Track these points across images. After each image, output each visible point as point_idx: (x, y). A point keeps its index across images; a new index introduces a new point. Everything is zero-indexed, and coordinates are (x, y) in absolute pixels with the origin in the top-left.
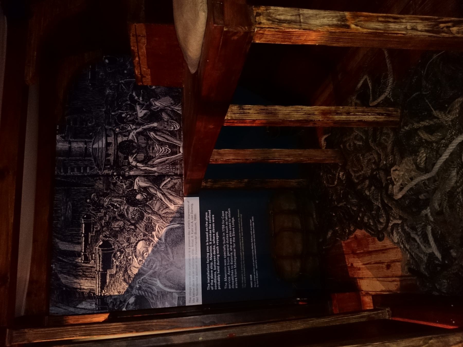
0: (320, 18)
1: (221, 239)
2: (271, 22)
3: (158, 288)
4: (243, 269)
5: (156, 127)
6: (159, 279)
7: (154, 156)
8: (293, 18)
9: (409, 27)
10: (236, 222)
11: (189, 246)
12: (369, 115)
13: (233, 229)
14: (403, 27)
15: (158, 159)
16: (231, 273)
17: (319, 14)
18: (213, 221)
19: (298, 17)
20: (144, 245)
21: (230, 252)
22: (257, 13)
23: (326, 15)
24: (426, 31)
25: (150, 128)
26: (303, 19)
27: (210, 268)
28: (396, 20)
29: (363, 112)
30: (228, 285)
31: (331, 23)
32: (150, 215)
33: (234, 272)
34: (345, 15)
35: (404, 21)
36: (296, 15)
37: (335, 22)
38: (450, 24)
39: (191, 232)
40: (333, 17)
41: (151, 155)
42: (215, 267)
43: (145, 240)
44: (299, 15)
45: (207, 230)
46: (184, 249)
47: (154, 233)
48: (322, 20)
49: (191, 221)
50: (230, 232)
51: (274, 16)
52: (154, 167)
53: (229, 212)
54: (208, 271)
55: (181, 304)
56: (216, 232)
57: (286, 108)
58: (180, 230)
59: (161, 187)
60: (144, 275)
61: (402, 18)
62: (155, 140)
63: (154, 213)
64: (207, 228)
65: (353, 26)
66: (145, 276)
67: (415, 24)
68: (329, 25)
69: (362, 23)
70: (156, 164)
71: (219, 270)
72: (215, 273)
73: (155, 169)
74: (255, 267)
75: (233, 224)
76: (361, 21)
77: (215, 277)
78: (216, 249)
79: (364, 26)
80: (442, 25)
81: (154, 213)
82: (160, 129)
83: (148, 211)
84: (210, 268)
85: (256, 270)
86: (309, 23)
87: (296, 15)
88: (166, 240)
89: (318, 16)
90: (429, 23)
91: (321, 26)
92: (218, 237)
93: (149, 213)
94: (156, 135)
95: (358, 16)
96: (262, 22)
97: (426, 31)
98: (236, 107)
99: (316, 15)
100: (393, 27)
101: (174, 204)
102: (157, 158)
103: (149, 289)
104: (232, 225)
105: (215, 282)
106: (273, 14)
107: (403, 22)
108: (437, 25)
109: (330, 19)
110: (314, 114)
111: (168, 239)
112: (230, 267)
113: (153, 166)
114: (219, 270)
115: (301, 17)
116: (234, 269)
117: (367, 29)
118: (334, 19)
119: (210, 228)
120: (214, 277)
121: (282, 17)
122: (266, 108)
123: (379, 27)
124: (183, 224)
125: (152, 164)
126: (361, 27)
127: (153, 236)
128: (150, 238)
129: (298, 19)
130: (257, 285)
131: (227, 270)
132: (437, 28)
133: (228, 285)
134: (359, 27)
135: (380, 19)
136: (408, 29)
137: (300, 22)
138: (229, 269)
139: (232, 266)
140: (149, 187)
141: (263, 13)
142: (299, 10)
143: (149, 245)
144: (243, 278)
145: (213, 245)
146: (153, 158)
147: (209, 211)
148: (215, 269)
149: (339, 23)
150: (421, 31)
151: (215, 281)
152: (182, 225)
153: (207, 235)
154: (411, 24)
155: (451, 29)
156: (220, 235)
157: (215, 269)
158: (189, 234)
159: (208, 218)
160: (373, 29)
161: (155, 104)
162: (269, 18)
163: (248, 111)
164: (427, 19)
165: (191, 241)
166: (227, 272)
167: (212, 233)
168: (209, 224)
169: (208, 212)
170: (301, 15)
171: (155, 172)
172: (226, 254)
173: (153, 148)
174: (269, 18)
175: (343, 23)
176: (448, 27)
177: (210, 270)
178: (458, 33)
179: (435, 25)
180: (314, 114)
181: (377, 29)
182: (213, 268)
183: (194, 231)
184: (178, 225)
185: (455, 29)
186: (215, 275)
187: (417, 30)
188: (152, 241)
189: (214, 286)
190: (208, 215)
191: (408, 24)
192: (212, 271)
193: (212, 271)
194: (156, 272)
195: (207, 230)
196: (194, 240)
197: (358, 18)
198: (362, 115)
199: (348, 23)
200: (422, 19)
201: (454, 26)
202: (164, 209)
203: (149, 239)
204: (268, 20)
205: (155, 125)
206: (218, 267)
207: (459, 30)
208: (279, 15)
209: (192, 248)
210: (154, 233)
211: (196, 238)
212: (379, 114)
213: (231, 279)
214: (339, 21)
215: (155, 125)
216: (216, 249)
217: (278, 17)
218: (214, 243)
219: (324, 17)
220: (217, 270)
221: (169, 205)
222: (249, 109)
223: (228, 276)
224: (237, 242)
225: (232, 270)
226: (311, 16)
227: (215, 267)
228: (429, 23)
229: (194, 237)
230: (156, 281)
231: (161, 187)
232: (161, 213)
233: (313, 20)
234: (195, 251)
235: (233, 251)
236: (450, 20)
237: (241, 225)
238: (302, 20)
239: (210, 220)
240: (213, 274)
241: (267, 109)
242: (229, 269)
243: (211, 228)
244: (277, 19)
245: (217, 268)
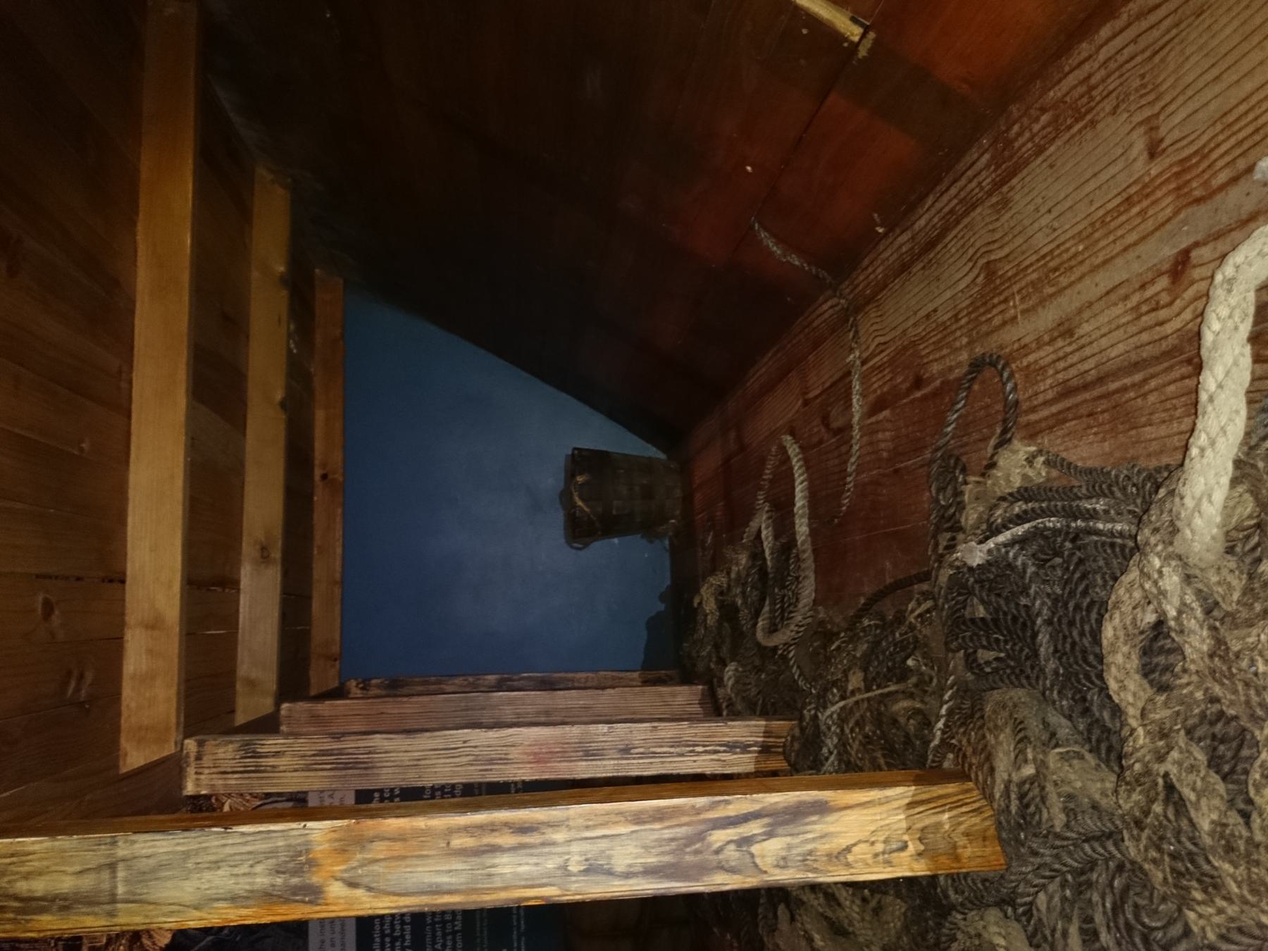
0: (198, 868)
4: (482, 932)
12: (699, 753)
14: (551, 864)
19: (106, 875)
23: (228, 850)
26: (127, 881)
27: (382, 931)
28: (526, 839)
29: (676, 743)
31: (242, 886)
33: (455, 943)
34: (308, 843)
35: (559, 836)
36: (98, 869)
37: (262, 881)
38: (754, 828)
42: (398, 927)
44: (112, 867)
48: (207, 875)
54: (378, 940)
57: (408, 741)
65: (336, 890)
67: (603, 844)
71: (408, 937)
72: (398, 944)
74: (519, 928)
79: (382, 886)
80: (719, 837)
84: (382, 931)
86: (151, 898)
90: (667, 834)
91: (196, 908)
97: (649, 872)
98: (231, 747)
99: (187, 855)
100: (507, 870)
107: (554, 844)
108: (700, 836)
109: (244, 869)
110: (505, 761)
112: (444, 928)
114: (408, 937)
115: (121, 874)
116: (454, 933)
117: (395, 894)
122: (336, 746)
123: (445, 879)
126: (370, 889)
129: (106, 886)
131: (434, 936)
132: (697, 852)
134: (359, 892)
135: (458, 842)
136: (570, 874)
137: (113, 899)
138: (439, 933)
139: (449, 926)
142: (114, 843)
148: (397, 934)
149: (279, 880)
150: (627, 875)
154: (586, 846)
155: (755, 849)
157: (397, 934)
163: (271, 761)
164: (659, 816)
166: (434, 943)
170: (121, 866)
175: (295, 881)
176: (745, 841)
177: (383, 936)
178: (783, 863)
179: (690, 840)
180: (505, 761)
182: (393, 930)
185: (774, 846)
187: (610, 873)
192: (387, 940)
193: (387, 940)
197: (363, 849)
198: (671, 754)
206: (408, 928)
207: (789, 847)
212: (731, 747)
217: (22, 887)
219: (216, 865)
220: (403, 936)
222: (277, 754)
225: (450, 937)
226: (161, 866)
227: (398, 927)
233: (169, 884)
236: (757, 807)
238: (121, 890)
241: (341, 752)
242: (439, 933)
244: (16, 898)
245: (402, 930)
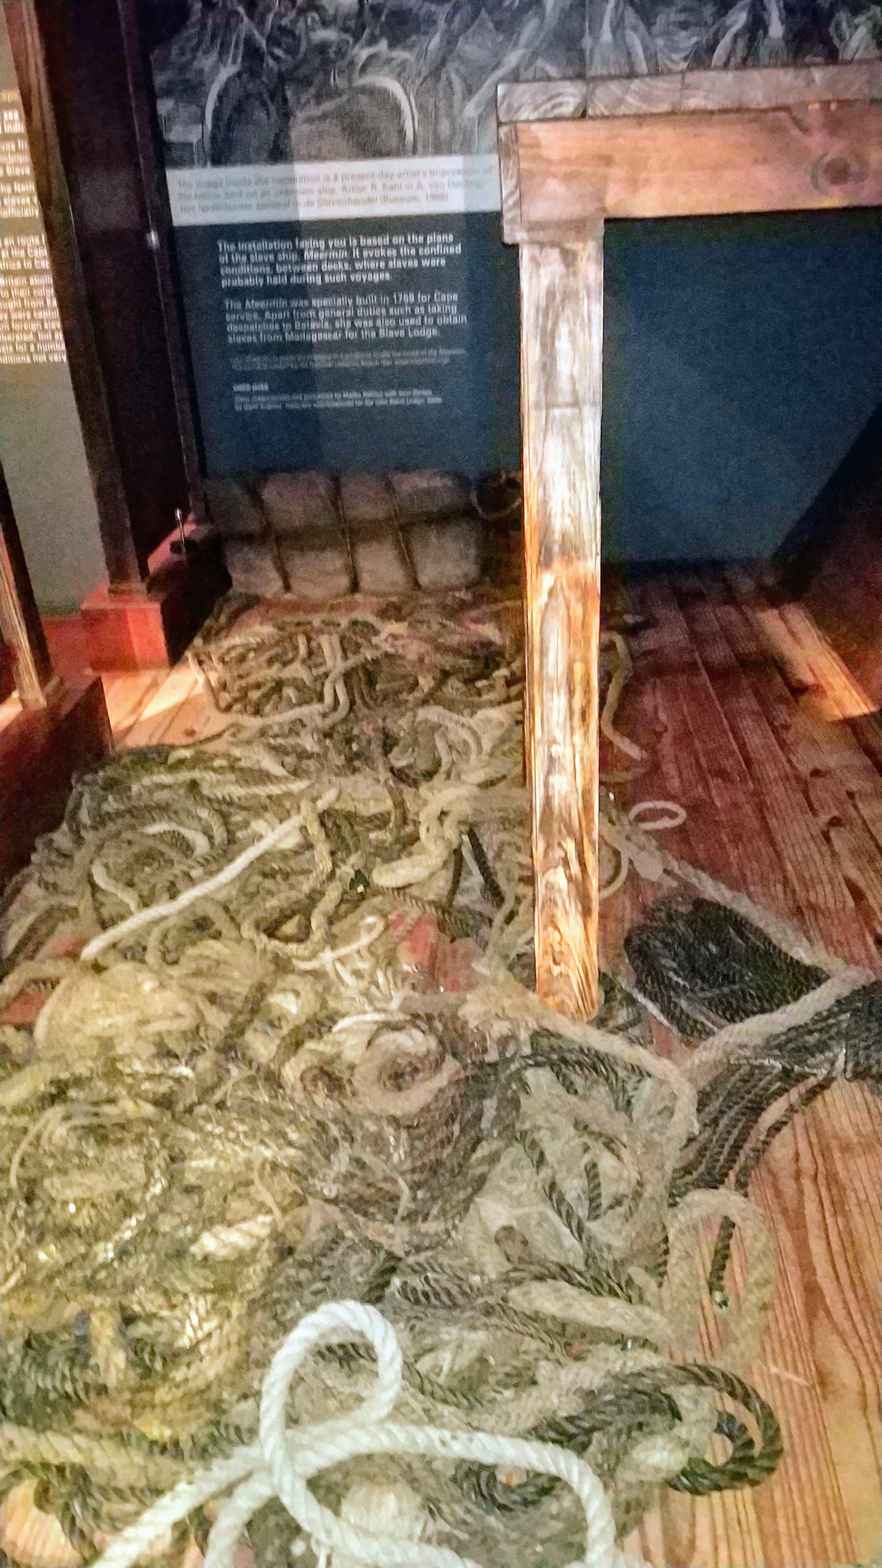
1: (365, 289)
2: (543, 303)
3: (215, 70)
5: (766, 31)
6: (239, 75)
7: (656, 29)
8: (563, 383)
9: (555, 750)
10: (421, 343)
11: (345, 177)
13: (402, 333)
15: (646, 49)
16: (269, 321)
17: (583, 472)
18: (425, 263)
20: (344, 10)
21: (332, 320)
22: (575, 255)
23: (583, 496)
24: (548, 801)
25: (764, 9)
26: (563, 416)
30: (235, 312)
32: (442, 24)
33: (274, 332)
35: (578, 738)
36: (574, 392)
38: (575, 869)
39: (389, 182)
40: (577, 520)
41: (661, 20)
43: (360, 13)
44: (576, 403)
45: (395, 241)
46: (335, 155)
47: (383, 45)
48: (564, 480)
49: (425, 182)
50: (392, 322)
51: (568, 312)
52: (614, 32)
53: (456, 321)
55: (175, 154)
56: (393, 271)
58: (393, 142)
59: (540, 62)
60: (251, 16)
61: (586, 733)
62: (716, 33)
63: (449, 42)
64: (401, 239)
66: (246, 19)
67: (570, 769)
68: (545, 502)
69: (563, 610)
70: (623, 37)
73: (606, 35)
75: (417, 333)
76: (568, 608)
77: (257, 270)
78: (338, 272)
79: (550, 613)
80: (570, 846)
81: (451, 41)
82: (757, 50)
83: (457, 19)
85: (284, 403)
87: (574, 392)
88: (363, 90)
89: (574, 467)
90: (574, 813)
92: (376, 278)
93: (449, 21)
94: (736, 36)
95: (584, 598)
96: (542, 271)
97: (548, 801)
99: (582, 464)
101: (480, 117)
102: (648, 38)
103: (208, 37)
104: (413, 327)
105: (243, 269)
106: (576, 314)
108: (571, 833)
109: (568, 509)
111: (364, 100)
113: (618, 27)
115: (568, 411)
118: (567, 521)
119: (404, 251)
120: (256, 264)
121: (563, 344)
124: (414, 152)
125: (627, 22)
127: (373, 41)
128: (367, 31)
130: (242, 404)
133: (235, 312)
134: (544, 598)
137: (549, 406)
140: (543, 18)
141: (575, 274)
143: (345, 29)
144: (259, 363)
145: (351, 261)
146: (649, 24)
147: (459, 249)
150: (546, 784)
151: (242, 268)
152: (409, 147)
153: (380, 241)
155: (560, 869)
156: (382, 288)
158: (383, 175)
159: (434, 244)
160: (542, 642)
161: (857, 27)
162: (558, 298)
165: (360, 183)
167: (387, 259)
168: (417, 246)
169: (455, 243)
171: (596, 38)
172: (323, 308)
173: (684, 26)
174: (558, 298)
175: (556, 549)
177: (275, 253)
178: (550, 886)
179: (568, 826)
181: (543, 654)
183: (391, 194)
184: (410, 135)
185: (559, 877)
186: (262, 269)
187: (549, 773)
188: (357, 39)
189: (230, 264)
190: (445, 244)
191: (569, 751)
194: (262, 60)
195: (395, 241)
196: (363, 196)
199: (557, 565)
200: (586, 794)
201: (570, 879)
202: (465, 80)
203: (364, 28)
204: (551, 294)
205: (776, 29)
208: (572, 333)
209: (338, 186)
210: (383, 45)
211: (370, 201)
213: (253, 322)
214: (563, 535)
215: (776, 29)
216: (338, 272)
217: (563, 329)
218: (358, 266)
219: (572, 487)
221: (476, 98)
223: (261, 312)
224: (362, 345)
228: (574, 813)
229: (373, 195)
230: (234, 61)
231: (540, 62)
232: (453, 73)
234: (328, 197)
235: (334, 330)
237: (417, 358)
238: (556, 412)
239: (427, 251)
240: (264, 263)
243: (402, 253)
244: (555, 324)
